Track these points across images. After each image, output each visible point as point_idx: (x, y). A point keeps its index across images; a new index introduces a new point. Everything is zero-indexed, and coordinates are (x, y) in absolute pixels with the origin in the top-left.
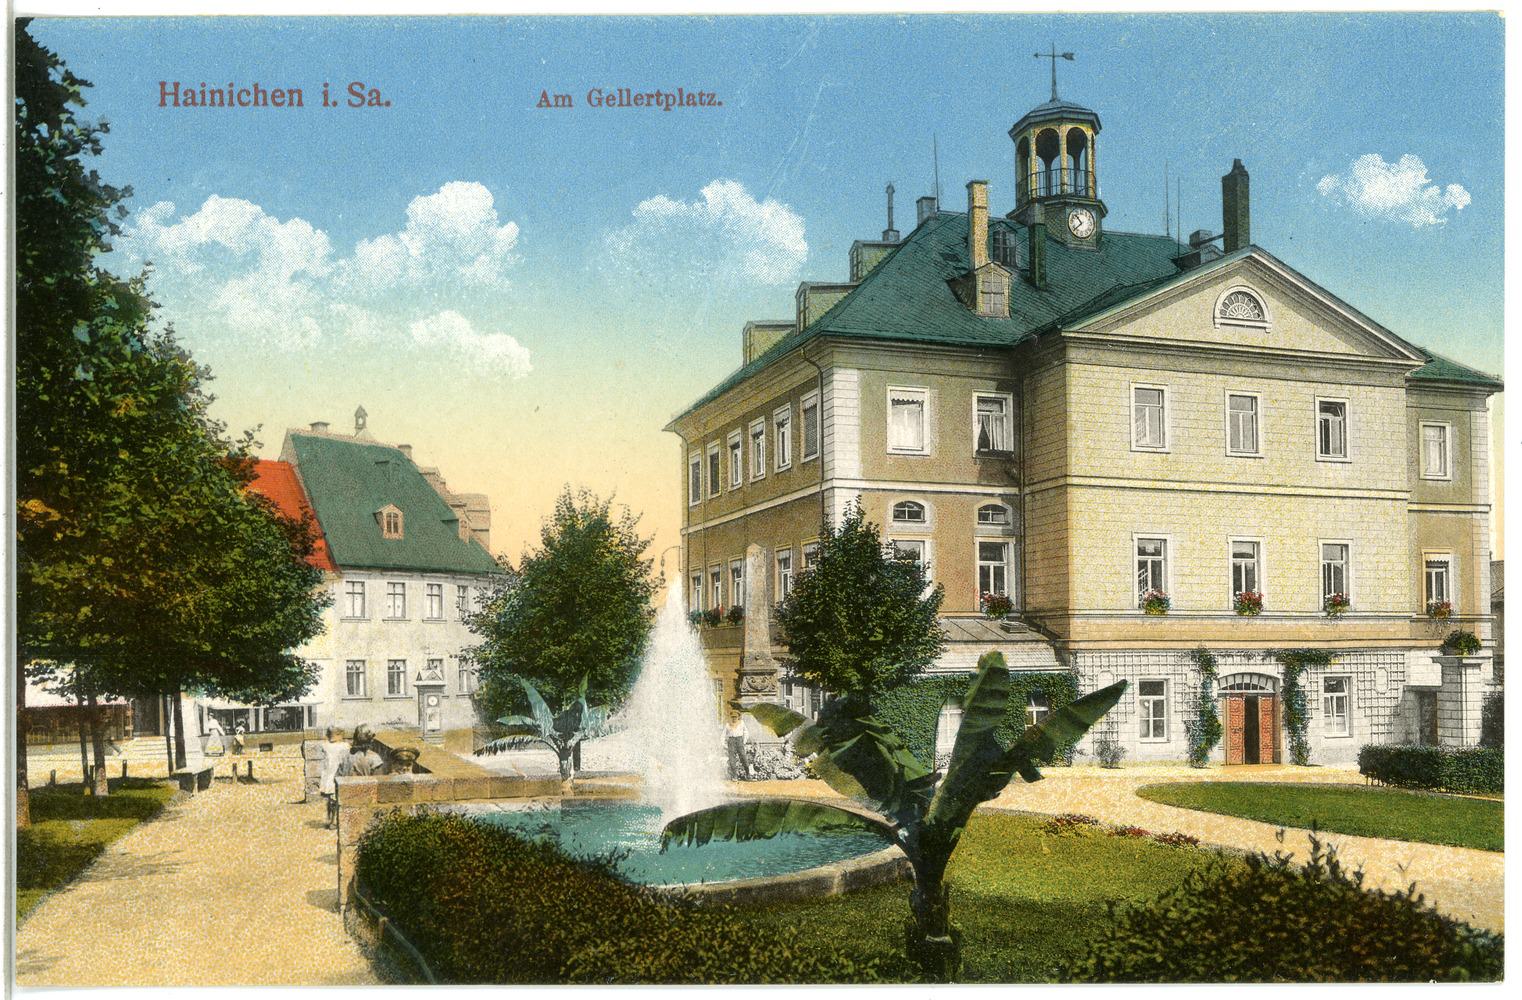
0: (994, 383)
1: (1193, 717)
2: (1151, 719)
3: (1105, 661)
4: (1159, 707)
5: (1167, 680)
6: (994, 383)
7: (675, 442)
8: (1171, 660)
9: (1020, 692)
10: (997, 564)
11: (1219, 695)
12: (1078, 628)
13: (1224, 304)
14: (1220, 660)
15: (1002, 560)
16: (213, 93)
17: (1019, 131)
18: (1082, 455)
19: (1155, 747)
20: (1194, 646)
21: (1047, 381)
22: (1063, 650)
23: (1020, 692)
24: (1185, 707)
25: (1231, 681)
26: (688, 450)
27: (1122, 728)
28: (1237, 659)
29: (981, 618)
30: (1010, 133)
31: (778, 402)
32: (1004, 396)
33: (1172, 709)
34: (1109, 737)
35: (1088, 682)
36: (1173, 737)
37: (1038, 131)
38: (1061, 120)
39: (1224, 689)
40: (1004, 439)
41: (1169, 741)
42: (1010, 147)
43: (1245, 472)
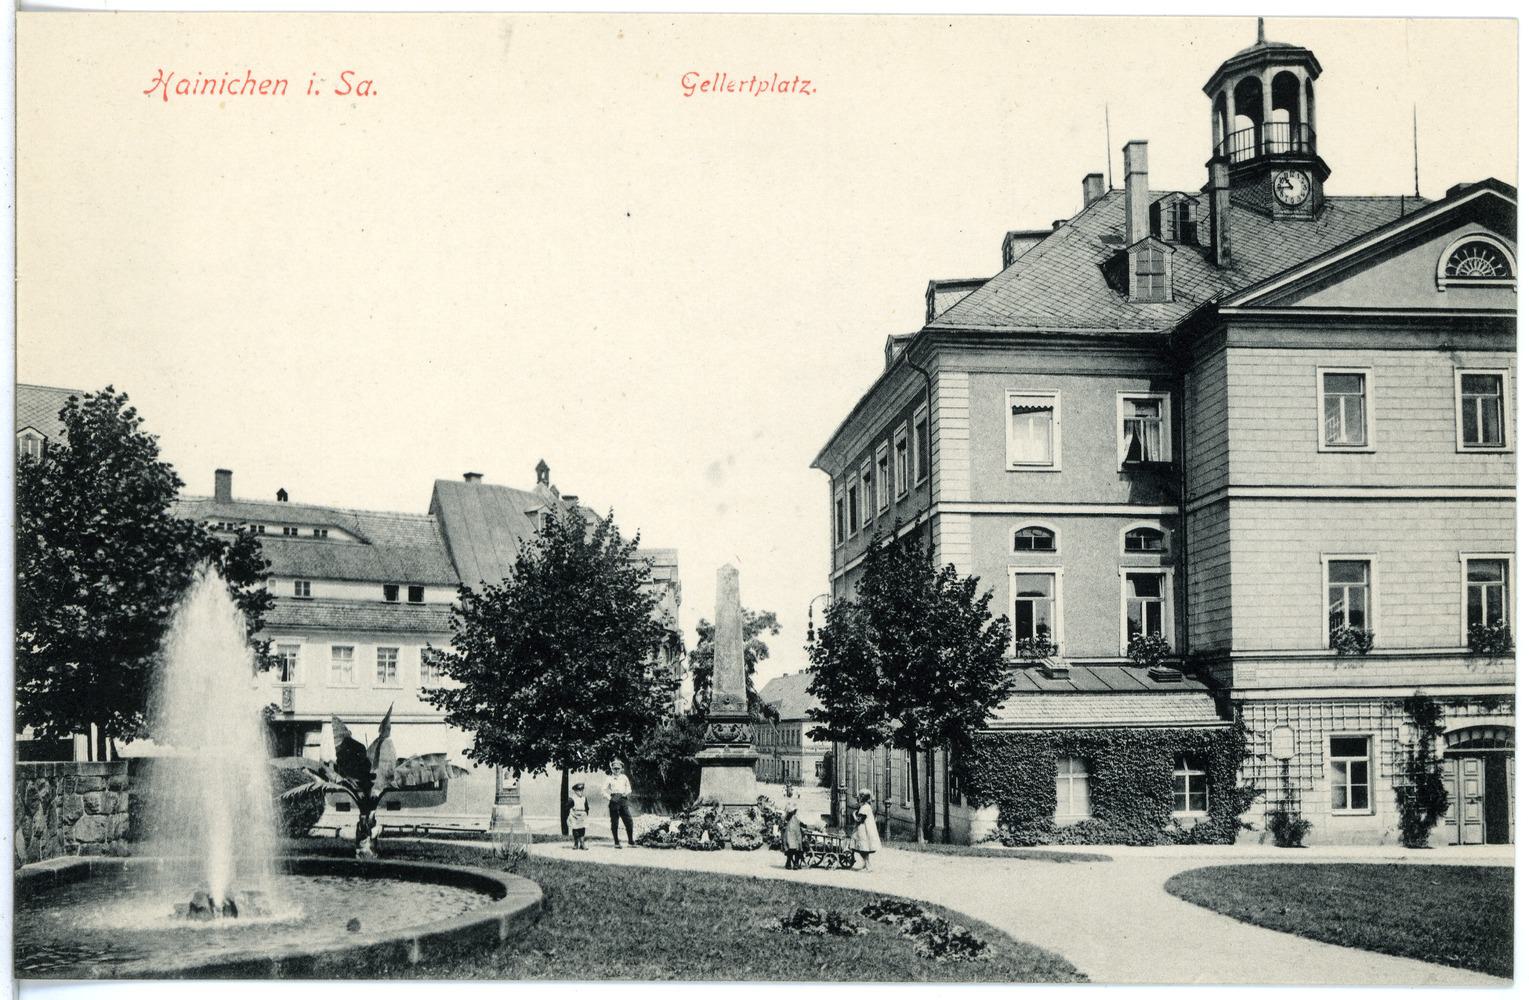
0: (1147, 383)
1: (1407, 782)
2: (1349, 786)
3: (1281, 714)
4: (1360, 772)
5: (1370, 736)
6: (1147, 383)
7: (822, 479)
8: (1376, 711)
9: (1164, 753)
10: (1153, 599)
11: (1446, 755)
12: (1244, 676)
13: (1452, 260)
14: (1447, 710)
15: (1158, 595)
17: (1213, 88)
18: (1247, 462)
19: (1352, 820)
20: (1410, 693)
21: (1208, 375)
22: (1226, 706)
23: (1164, 753)
24: (1397, 771)
25: (1464, 738)
26: (834, 484)
27: (1305, 796)
28: (1473, 709)
29: (1127, 664)
30: (1204, 89)
31: (895, 423)
32: (1160, 396)
33: (1378, 773)
34: (1288, 808)
35: (1258, 740)
36: (1379, 808)
37: (1236, 82)
38: (1264, 65)
39: (1455, 747)
40: (1159, 449)
41: (1373, 813)
42: (1207, 103)
43: (1485, 474)
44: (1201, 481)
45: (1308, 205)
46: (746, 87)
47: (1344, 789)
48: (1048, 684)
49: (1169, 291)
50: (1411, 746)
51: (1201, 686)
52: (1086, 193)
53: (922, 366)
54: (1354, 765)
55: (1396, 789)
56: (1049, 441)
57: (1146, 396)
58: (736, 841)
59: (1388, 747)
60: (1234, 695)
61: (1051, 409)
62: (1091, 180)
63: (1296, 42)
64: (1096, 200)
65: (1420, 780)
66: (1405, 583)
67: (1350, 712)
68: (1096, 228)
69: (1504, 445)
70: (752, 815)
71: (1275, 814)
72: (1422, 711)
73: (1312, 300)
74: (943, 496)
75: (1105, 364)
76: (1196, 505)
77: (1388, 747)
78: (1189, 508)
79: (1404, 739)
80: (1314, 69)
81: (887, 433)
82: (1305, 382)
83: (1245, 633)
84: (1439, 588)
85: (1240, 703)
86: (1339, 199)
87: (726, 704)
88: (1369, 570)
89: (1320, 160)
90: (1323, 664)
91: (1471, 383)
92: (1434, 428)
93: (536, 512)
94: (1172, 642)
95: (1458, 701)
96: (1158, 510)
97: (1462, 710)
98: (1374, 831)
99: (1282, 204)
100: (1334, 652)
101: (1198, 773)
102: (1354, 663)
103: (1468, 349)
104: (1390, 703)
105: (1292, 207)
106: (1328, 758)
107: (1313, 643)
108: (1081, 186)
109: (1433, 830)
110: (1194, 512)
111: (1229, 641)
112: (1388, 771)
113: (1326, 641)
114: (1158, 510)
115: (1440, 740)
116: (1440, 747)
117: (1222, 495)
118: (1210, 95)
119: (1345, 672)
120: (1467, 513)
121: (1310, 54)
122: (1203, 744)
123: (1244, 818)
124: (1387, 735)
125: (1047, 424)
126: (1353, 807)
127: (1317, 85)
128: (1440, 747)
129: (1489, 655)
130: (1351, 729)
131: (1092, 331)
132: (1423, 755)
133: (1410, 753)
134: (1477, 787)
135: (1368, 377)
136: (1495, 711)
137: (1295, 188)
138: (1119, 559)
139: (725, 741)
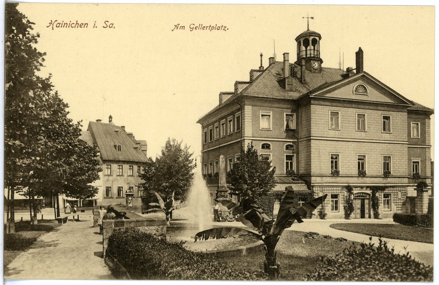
4: (336, 202)
5: (339, 194)
6: (290, 110)
10: (291, 161)
11: (354, 199)
12: (314, 180)
14: (354, 189)
16: (65, 24)
18: (315, 131)
19: (335, 213)
20: (347, 185)
25: (357, 195)
28: (359, 189)
29: (286, 176)
30: (295, 39)
34: (322, 210)
35: (316, 195)
36: (340, 211)
39: (355, 197)
41: (339, 212)
42: (296, 43)
44: (303, 133)
45: (319, 69)
46: (208, 28)
47: (333, 206)
48: (294, 182)
49: (294, 89)
50: (347, 197)
51: (304, 182)
52: (270, 62)
53: (239, 103)
54: (335, 201)
55: (344, 206)
56: (269, 122)
57: (290, 114)
58: (229, 220)
59: (342, 197)
60: (312, 184)
61: (270, 116)
62: (271, 59)
63: (317, 31)
64: (272, 63)
65: (349, 204)
66: (346, 160)
67: (335, 189)
68: (274, 71)
69: (365, 130)
70: (230, 213)
71: (319, 212)
72: (349, 189)
73: (328, 95)
74: (246, 135)
75: (285, 106)
76: (302, 140)
77: (342, 197)
78: (300, 140)
79: (346, 195)
80: (320, 38)
81: (225, 117)
82: (379, 117)
83: (314, 170)
84: (375, 165)
85: (313, 186)
86: (326, 68)
87: (222, 188)
88: (339, 157)
89: (321, 59)
90: (329, 178)
91: (385, 118)
92: (352, 125)
93: (118, 131)
94: (295, 171)
95: (356, 187)
96: (292, 140)
97: (357, 189)
98: (339, 216)
99: (314, 69)
100: (332, 175)
101: (303, 202)
102: (336, 178)
103: (270, 98)
104: (343, 187)
105: (316, 69)
106: (330, 199)
107: (328, 173)
108: (268, 60)
109: (351, 215)
110: (301, 141)
111: (311, 172)
112: (342, 202)
113: (330, 172)
114: (292, 140)
115: (352, 195)
116: (352, 197)
117: (309, 138)
118: (297, 41)
119: (333, 180)
120: (364, 145)
121: (320, 35)
122: (305, 196)
123: (313, 213)
124: (342, 194)
125: (269, 119)
126: (335, 210)
127: (320, 41)
128: (352, 197)
129: (362, 177)
130: (335, 192)
131: (280, 98)
132: (349, 199)
133: (347, 198)
134: (359, 206)
135: (366, 115)
136: (363, 189)
137: (316, 65)
138: (284, 151)
139: (223, 196)
